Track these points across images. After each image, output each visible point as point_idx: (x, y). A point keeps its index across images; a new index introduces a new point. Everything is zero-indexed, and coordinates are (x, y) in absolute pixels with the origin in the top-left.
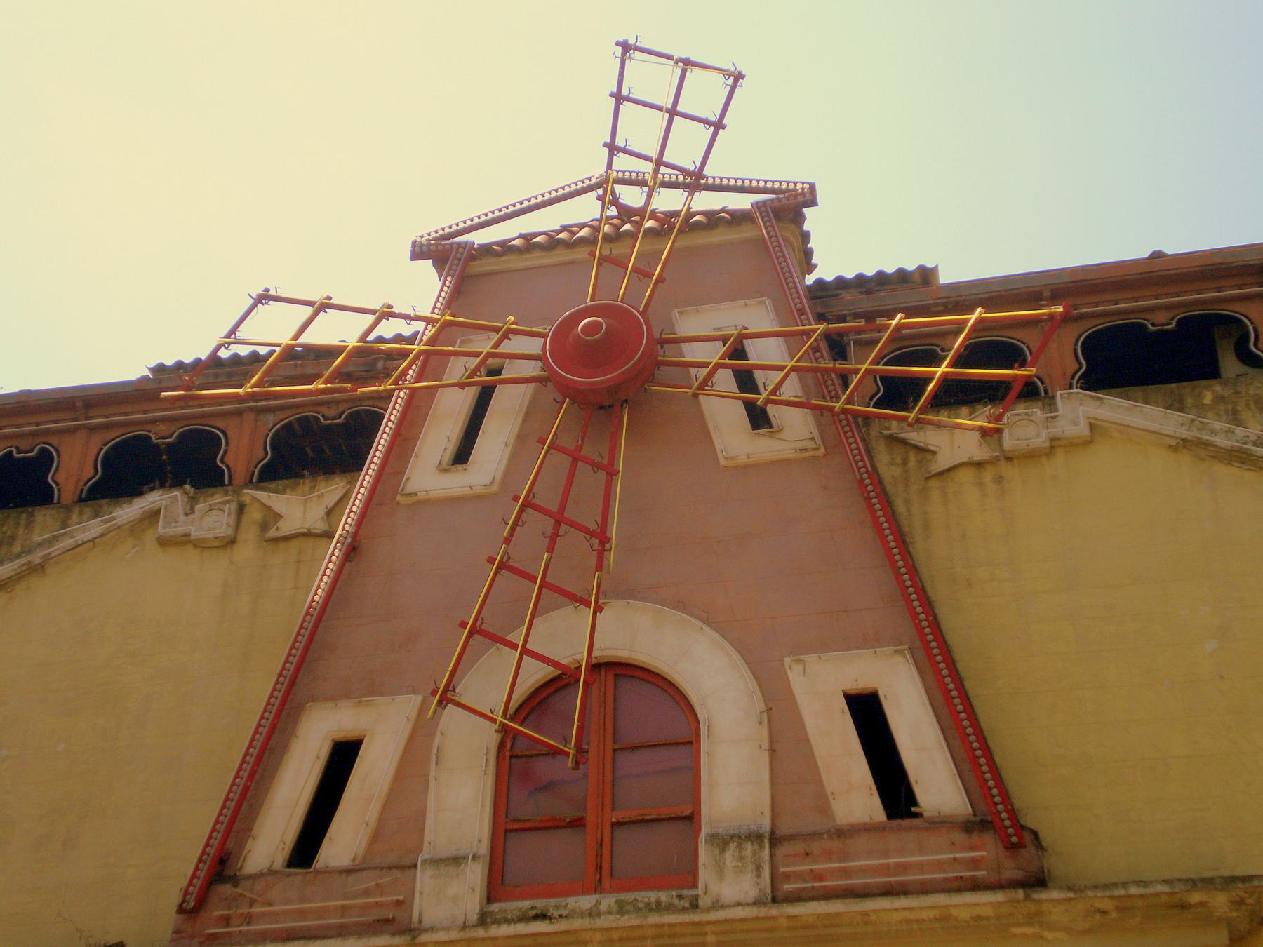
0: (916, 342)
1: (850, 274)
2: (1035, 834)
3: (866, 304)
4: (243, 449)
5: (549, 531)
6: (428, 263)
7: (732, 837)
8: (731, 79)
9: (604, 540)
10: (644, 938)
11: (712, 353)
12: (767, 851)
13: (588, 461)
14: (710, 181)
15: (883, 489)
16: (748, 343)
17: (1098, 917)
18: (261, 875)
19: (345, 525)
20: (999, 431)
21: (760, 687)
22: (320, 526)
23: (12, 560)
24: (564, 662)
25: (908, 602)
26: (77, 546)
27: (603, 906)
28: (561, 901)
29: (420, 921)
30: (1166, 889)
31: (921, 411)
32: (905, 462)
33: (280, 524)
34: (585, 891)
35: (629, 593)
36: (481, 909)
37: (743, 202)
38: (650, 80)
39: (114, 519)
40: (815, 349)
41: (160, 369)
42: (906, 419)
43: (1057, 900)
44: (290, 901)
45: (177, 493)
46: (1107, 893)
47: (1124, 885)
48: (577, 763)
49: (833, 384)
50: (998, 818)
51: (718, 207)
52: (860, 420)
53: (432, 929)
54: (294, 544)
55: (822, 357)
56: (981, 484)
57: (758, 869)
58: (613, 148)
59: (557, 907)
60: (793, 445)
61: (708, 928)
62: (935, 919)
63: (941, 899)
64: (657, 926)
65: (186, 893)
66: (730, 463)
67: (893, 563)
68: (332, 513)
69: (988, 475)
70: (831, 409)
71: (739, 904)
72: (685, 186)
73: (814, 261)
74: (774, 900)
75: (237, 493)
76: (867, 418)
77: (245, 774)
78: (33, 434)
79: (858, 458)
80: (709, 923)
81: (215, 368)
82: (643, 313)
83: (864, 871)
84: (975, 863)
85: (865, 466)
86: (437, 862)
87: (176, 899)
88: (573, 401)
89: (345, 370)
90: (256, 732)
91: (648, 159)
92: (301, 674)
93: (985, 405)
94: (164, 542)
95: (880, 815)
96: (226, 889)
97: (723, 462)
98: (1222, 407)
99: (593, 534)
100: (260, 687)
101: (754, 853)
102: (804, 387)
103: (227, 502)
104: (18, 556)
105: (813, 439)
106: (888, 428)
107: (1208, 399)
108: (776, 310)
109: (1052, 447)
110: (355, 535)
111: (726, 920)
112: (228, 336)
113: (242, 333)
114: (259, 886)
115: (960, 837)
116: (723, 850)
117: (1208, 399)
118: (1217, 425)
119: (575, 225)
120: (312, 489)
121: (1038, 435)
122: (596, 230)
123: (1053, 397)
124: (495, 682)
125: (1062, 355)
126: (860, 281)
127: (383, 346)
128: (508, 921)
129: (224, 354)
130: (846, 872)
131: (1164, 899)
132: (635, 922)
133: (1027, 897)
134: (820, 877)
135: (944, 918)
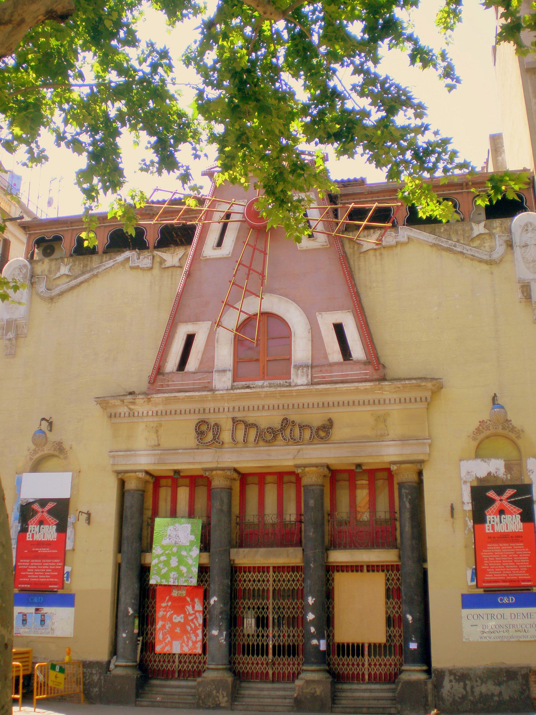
4: (152, 237)
9: (263, 276)
13: (258, 249)
18: (170, 373)
22: (177, 264)
32: (354, 248)
35: (272, 291)
44: (178, 380)
45: (134, 252)
50: (374, 360)
53: (218, 390)
54: (170, 269)
56: (375, 256)
57: (308, 375)
63: (356, 384)
69: (378, 253)
83: (336, 376)
84: (366, 374)
86: (218, 371)
94: (132, 268)
95: (341, 360)
96: (161, 377)
99: (260, 274)
100: (165, 316)
110: (189, 271)
114: (170, 376)
124: (232, 319)
128: (239, 388)
134: (324, 377)
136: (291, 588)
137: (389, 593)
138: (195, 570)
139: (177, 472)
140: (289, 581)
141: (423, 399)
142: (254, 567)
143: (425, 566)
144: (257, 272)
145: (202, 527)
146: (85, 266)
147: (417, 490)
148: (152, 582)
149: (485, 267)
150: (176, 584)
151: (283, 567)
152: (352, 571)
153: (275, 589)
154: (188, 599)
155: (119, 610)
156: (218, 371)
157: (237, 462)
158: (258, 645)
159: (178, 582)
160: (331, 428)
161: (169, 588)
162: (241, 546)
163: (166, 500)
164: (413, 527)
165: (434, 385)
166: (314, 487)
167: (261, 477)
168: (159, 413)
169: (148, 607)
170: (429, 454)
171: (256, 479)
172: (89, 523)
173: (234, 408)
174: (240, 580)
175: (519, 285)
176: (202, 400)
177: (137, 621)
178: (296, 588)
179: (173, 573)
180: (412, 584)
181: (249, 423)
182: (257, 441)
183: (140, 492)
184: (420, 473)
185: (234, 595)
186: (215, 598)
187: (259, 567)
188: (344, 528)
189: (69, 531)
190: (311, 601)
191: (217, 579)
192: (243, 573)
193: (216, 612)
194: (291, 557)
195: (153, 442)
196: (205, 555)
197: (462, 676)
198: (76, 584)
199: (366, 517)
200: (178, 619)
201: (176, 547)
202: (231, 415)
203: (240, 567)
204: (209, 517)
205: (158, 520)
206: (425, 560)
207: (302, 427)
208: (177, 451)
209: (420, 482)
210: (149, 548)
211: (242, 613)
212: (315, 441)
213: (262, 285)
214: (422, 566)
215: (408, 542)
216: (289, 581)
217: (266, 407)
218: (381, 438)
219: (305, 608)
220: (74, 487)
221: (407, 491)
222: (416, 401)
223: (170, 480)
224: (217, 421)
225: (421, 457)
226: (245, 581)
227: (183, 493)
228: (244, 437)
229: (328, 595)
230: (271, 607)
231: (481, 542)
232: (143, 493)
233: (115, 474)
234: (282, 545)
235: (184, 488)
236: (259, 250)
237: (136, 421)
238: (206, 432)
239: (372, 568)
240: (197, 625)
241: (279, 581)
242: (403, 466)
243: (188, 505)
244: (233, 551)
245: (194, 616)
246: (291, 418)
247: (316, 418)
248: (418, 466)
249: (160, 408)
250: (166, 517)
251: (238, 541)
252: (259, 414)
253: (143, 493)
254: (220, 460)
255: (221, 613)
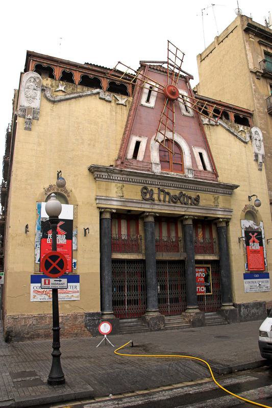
84: (213, 178)
149: (243, 144)
158: (120, 291)
175: (254, 154)
189: (74, 239)
197: (247, 306)
198: (79, 270)
220: (75, 214)
231: (248, 253)
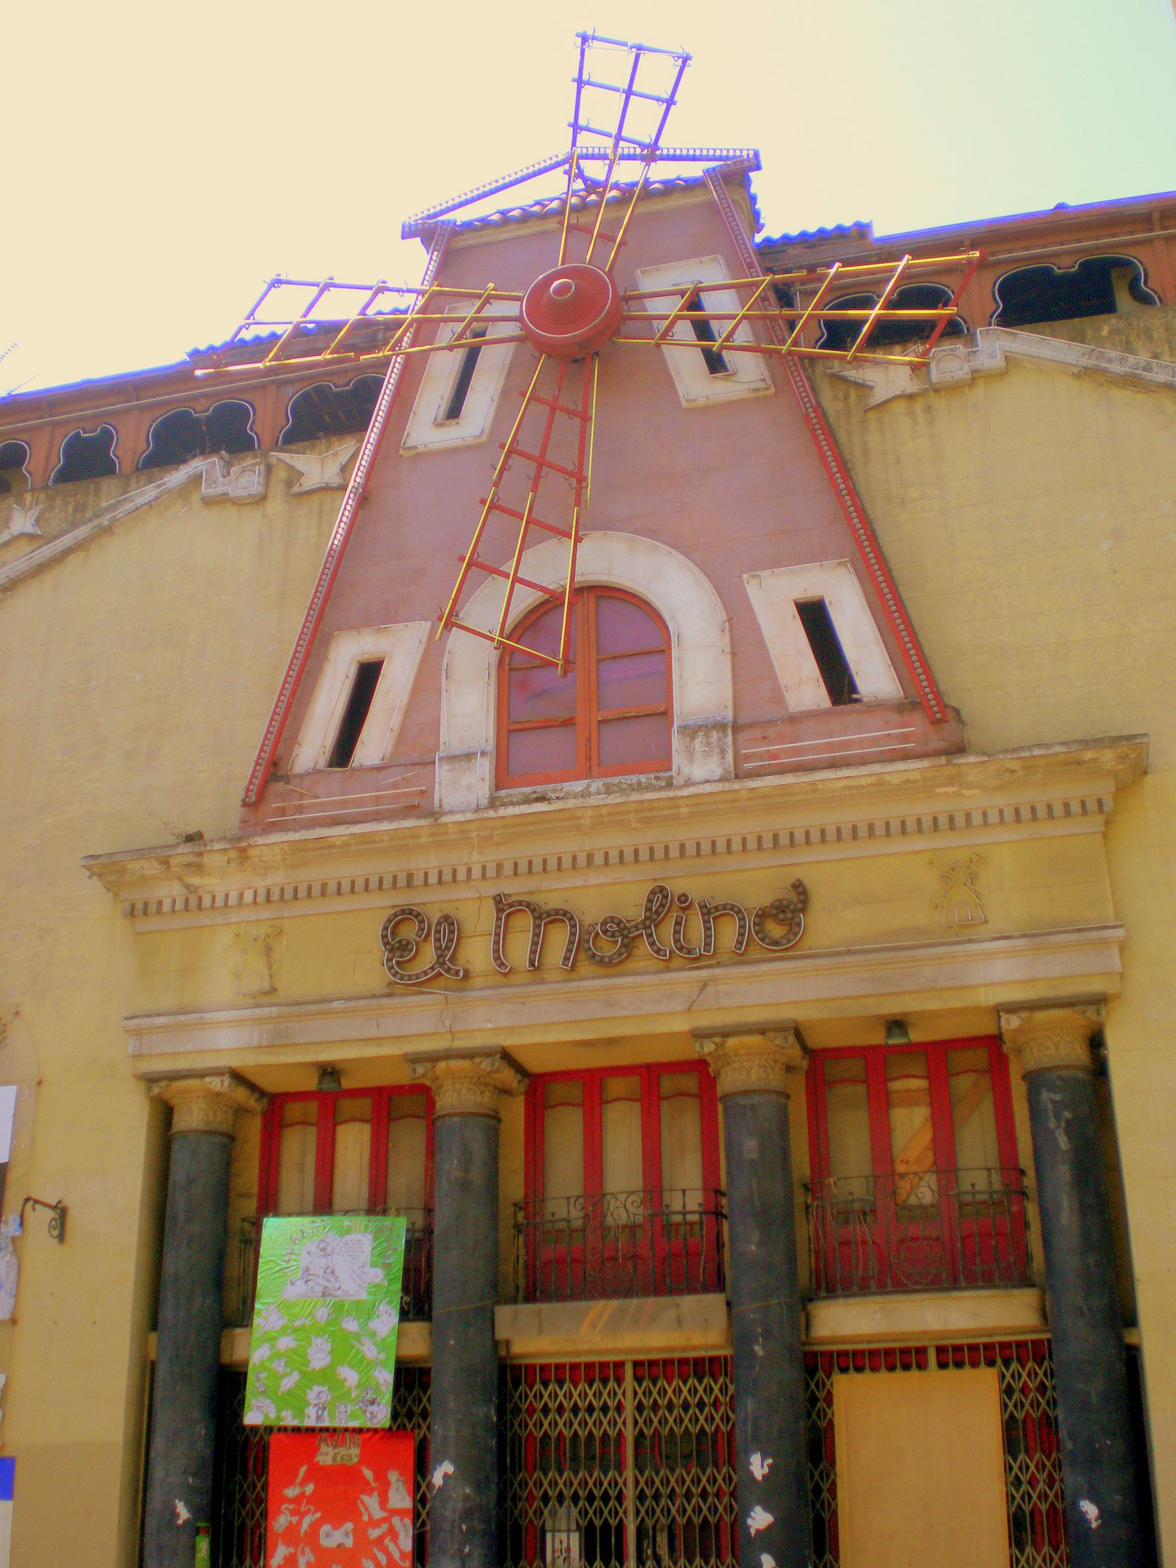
0: (852, 290)
1: (794, 232)
2: (957, 712)
3: (810, 258)
4: (268, 417)
5: (533, 474)
6: (417, 241)
7: (700, 727)
8: (681, 60)
9: (581, 479)
10: (629, 812)
11: (670, 307)
12: (730, 737)
14: (665, 152)
15: (827, 422)
16: (703, 296)
17: (1007, 775)
18: (307, 774)
19: (357, 478)
20: (927, 365)
21: (722, 600)
22: (336, 481)
23: (84, 523)
24: (551, 587)
25: (849, 519)
26: (137, 509)
27: (593, 789)
28: (559, 786)
29: (441, 806)
30: (1063, 749)
31: (859, 350)
32: (846, 399)
33: (302, 480)
34: (579, 778)
35: (606, 525)
36: (491, 794)
37: (694, 170)
38: (609, 66)
39: (165, 484)
40: (763, 299)
41: (195, 353)
42: (845, 357)
43: (973, 763)
44: (334, 791)
45: (215, 459)
46: (1015, 756)
47: (1029, 748)
48: (565, 673)
49: (781, 329)
51: (673, 176)
52: (806, 361)
53: (451, 812)
54: (315, 498)
55: (770, 305)
56: (912, 414)
57: (723, 752)
58: (576, 127)
59: (554, 791)
60: (747, 386)
61: (681, 802)
62: (872, 785)
63: (877, 768)
64: (638, 802)
65: (248, 790)
66: (691, 405)
67: (835, 487)
68: (345, 469)
69: (919, 406)
70: (778, 352)
71: (707, 781)
72: (642, 158)
73: (762, 221)
74: (737, 777)
75: (265, 456)
76: (812, 359)
77: (287, 693)
78: (96, 416)
79: (804, 394)
80: (682, 797)
81: (238, 349)
82: (609, 274)
83: (812, 749)
84: (906, 738)
85: (810, 402)
86: (451, 759)
87: (241, 794)
88: (549, 356)
89: (345, 343)
90: (294, 657)
91: (610, 136)
92: (327, 609)
93: (915, 343)
94: (208, 502)
96: (280, 786)
97: (684, 404)
98: (1117, 338)
99: (571, 474)
100: (295, 622)
101: (719, 740)
102: (755, 334)
103: (258, 464)
104: (90, 520)
105: (764, 380)
106: (830, 368)
107: (1105, 332)
108: (727, 263)
109: (973, 379)
110: (365, 486)
111: (696, 795)
112: (248, 318)
113: (258, 315)
114: (307, 782)
115: (894, 717)
116: (692, 739)
117: (1105, 332)
118: (1113, 354)
119: (547, 200)
120: (328, 449)
121: (961, 368)
122: (564, 202)
123: (975, 334)
124: (492, 607)
125: (983, 296)
126: (803, 238)
127: (380, 318)
128: (513, 804)
129: (247, 335)
130: (797, 751)
131: (1062, 757)
132: (620, 800)
133: (948, 763)
135: (880, 783)
136: (695, 1430)
137: (1014, 1436)
138: (386, 1377)
139: (329, 1071)
140: (684, 1407)
141: (1092, 806)
142: (574, 1367)
143: (1131, 1338)
144: (563, 471)
145: (408, 1242)
146: (80, 508)
147: (1091, 1088)
148: (252, 1417)
150: (327, 1423)
151: (667, 1362)
152: (891, 1368)
153: (641, 1432)
154: (368, 1474)
155: (149, 1508)
156: (451, 759)
157: (511, 1030)
159: (331, 1417)
160: (803, 910)
161: (308, 1436)
162: (531, 1296)
163: (301, 1168)
164: (1084, 1211)
165: (1122, 758)
166: (756, 1099)
167: (591, 1085)
168: (275, 896)
169: (244, 1501)
170: (1121, 975)
171: (574, 1091)
172: (61, 1238)
173: (499, 867)
174: (531, 1411)
176: (403, 845)
177: (203, 1545)
178: (710, 1429)
179: (316, 1389)
180: (1094, 1400)
181: (547, 908)
182: (571, 965)
183: (217, 1139)
184: (1096, 1042)
185: (511, 1458)
186: (447, 1467)
187: (589, 1366)
188: (858, 1230)
190: (758, 1466)
191: (452, 1405)
192: (538, 1386)
193: (450, 1511)
194: (688, 1325)
195: (258, 983)
196: (418, 1329)
199: (925, 1192)
200: (336, 1537)
201: (325, 1308)
202: (490, 889)
203: (531, 1368)
204: (429, 1211)
205: (272, 1227)
206: (1129, 1319)
207: (712, 913)
208: (327, 1006)
209: (1099, 1070)
210: (243, 1316)
211: (539, 1513)
212: (756, 953)
213: (578, 503)
214: (1120, 1338)
215: (1070, 1261)
216: (686, 1406)
217: (599, 859)
218: (963, 931)
219: (739, 1495)
221: (1058, 1097)
222: (1068, 813)
223: (313, 1107)
224: (449, 910)
225: (1096, 986)
226: (546, 1410)
227: (353, 1144)
228: (533, 952)
229: (814, 1450)
230: (630, 1493)
232: (228, 1141)
233: (142, 1086)
234: (660, 1288)
235: (358, 1126)
236: (567, 411)
237: (207, 922)
238: (417, 946)
239: (956, 1355)
240: (397, 1555)
241: (655, 1407)
242: (1040, 1016)
243: (366, 1180)
244: (504, 1313)
245: (385, 1527)
246: (677, 886)
247: (755, 883)
248: (1090, 1012)
249: (277, 879)
250: (301, 1213)
251: (522, 1282)
252: (576, 880)
253: (228, 1141)
254: (458, 1027)
255: (467, 1514)
